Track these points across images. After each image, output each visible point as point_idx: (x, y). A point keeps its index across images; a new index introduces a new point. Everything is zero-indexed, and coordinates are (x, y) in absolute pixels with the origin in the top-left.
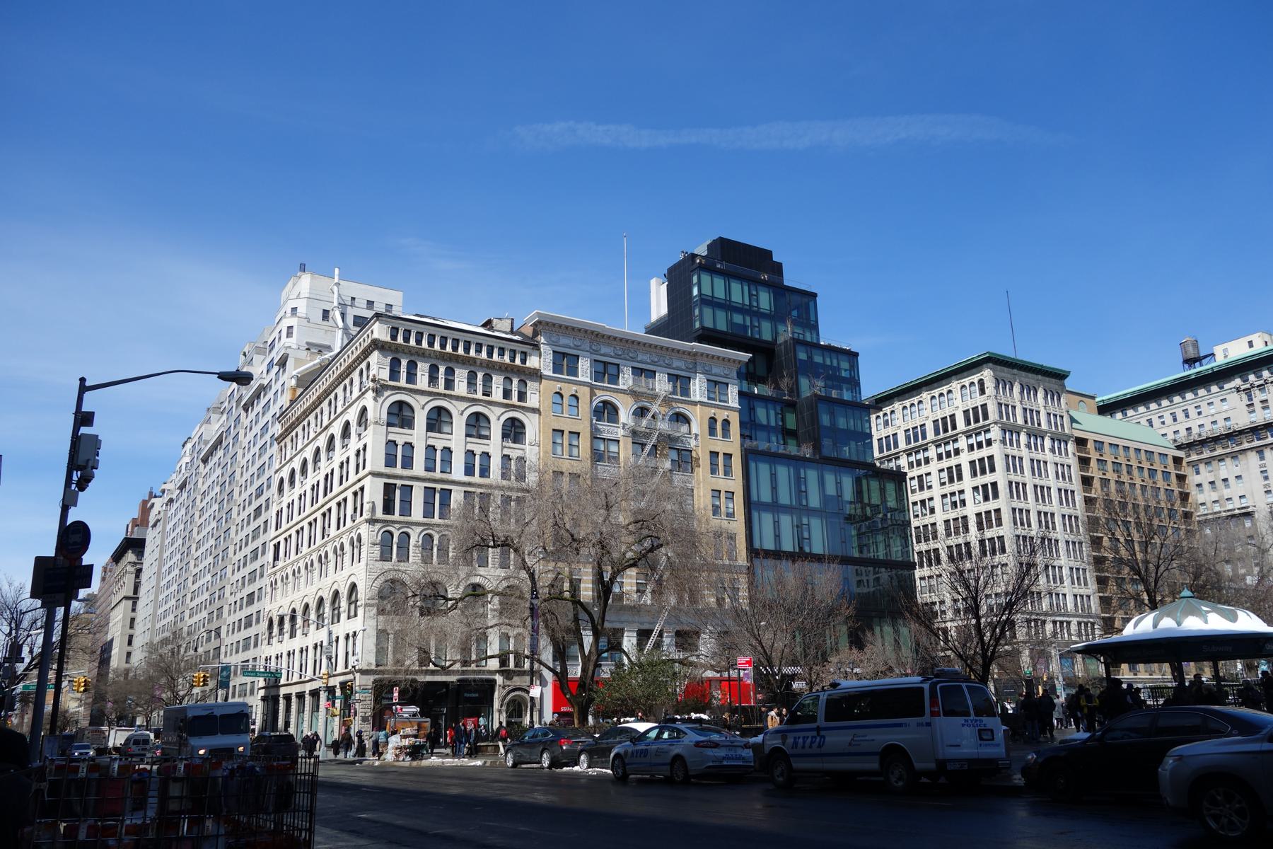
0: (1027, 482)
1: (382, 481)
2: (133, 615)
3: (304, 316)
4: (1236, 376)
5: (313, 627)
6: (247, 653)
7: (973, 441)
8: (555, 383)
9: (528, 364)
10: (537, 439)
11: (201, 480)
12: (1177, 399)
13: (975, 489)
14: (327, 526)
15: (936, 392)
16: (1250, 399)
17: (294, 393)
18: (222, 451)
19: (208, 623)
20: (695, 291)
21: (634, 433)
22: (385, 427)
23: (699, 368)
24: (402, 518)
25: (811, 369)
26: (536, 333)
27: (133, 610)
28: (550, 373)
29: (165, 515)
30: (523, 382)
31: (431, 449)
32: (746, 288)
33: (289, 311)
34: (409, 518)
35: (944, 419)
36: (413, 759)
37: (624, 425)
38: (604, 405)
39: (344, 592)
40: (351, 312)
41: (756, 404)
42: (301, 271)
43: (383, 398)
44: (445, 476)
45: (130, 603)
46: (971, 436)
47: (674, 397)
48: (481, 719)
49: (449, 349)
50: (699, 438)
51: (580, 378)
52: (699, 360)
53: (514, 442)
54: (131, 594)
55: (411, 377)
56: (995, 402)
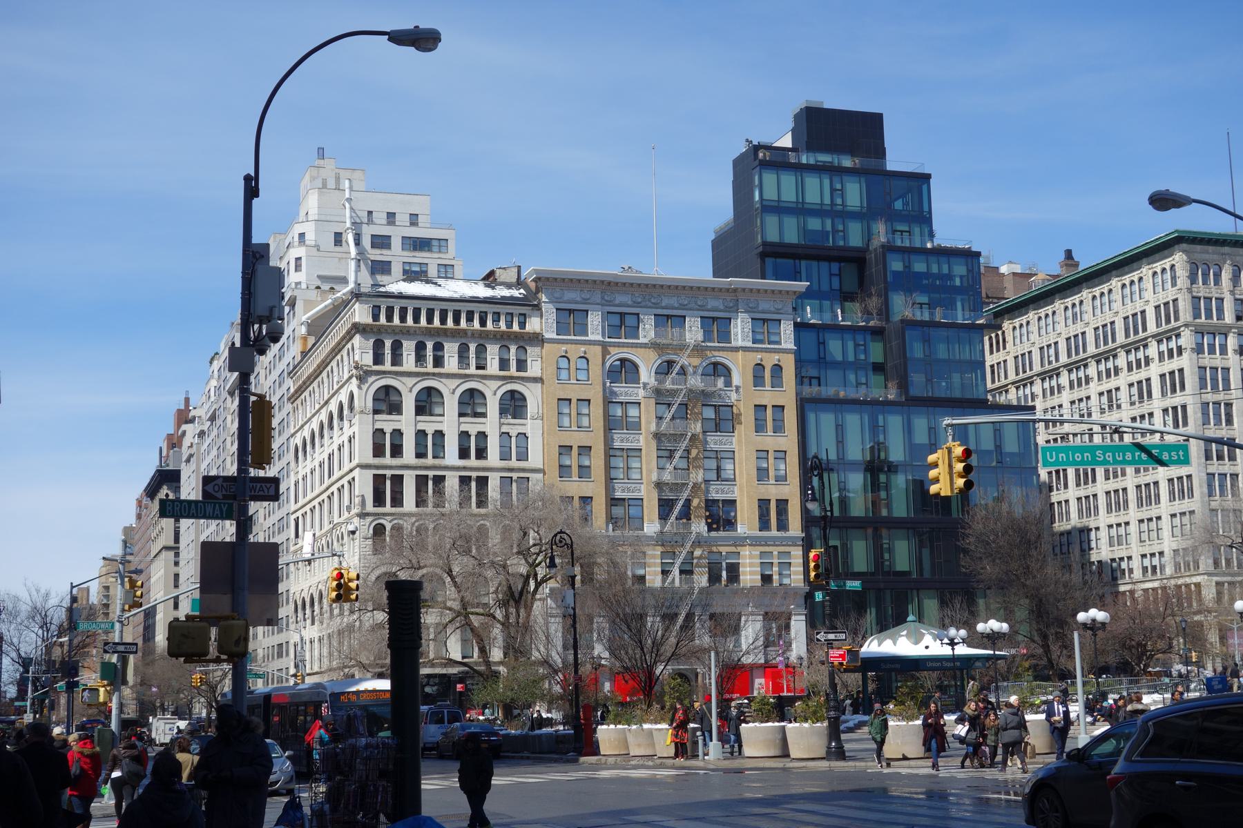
2: (176, 570)
6: (281, 635)
10: (540, 411)
13: (1165, 411)
17: (305, 343)
21: (658, 392)
22: (371, 415)
25: (909, 282)
27: (176, 564)
29: (198, 450)
30: (522, 348)
31: (421, 434)
32: (827, 182)
37: (645, 385)
38: (621, 363)
40: (367, 232)
41: (828, 335)
44: (437, 462)
45: (171, 554)
47: (709, 344)
50: (741, 390)
51: (591, 337)
53: (514, 418)
54: (171, 543)
56: (1188, 297)
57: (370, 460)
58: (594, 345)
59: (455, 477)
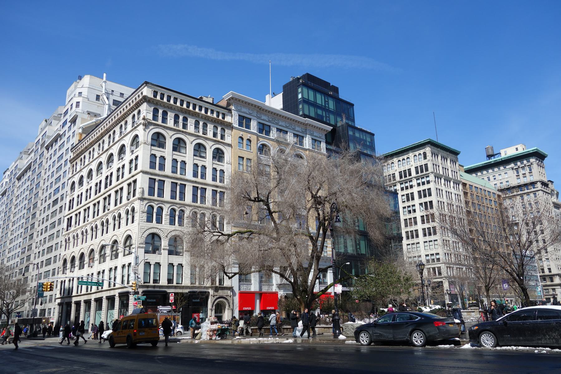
0: (445, 202)
1: (148, 177)
3: (86, 97)
4: (512, 163)
5: (77, 268)
7: (403, 186)
8: (240, 132)
9: (226, 120)
10: (231, 161)
11: (16, 189)
12: (485, 172)
13: (421, 204)
14: (87, 215)
15: (401, 158)
16: (518, 173)
18: (31, 172)
19: (20, 264)
20: (300, 96)
22: (150, 146)
23: (308, 132)
24: (159, 199)
26: (229, 104)
28: (237, 126)
31: (175, 161)
32: (323, 97)
33: (77, 94)
34: (163, 199)
35: (405, 171)
36: (222, 339)
39: (121, 240)
40: (112, 98)
42: (79, 79)
43: (149, 130)
44: (182, 177)
46: (403, 183)
48: (201, 314)
49: (185, 106)
51: (252, 130)
52: (308, 128)
53: (219, 161)
55: (164, 120)
57: (148, 169)
58: (254, 135)
59: (191, 186)
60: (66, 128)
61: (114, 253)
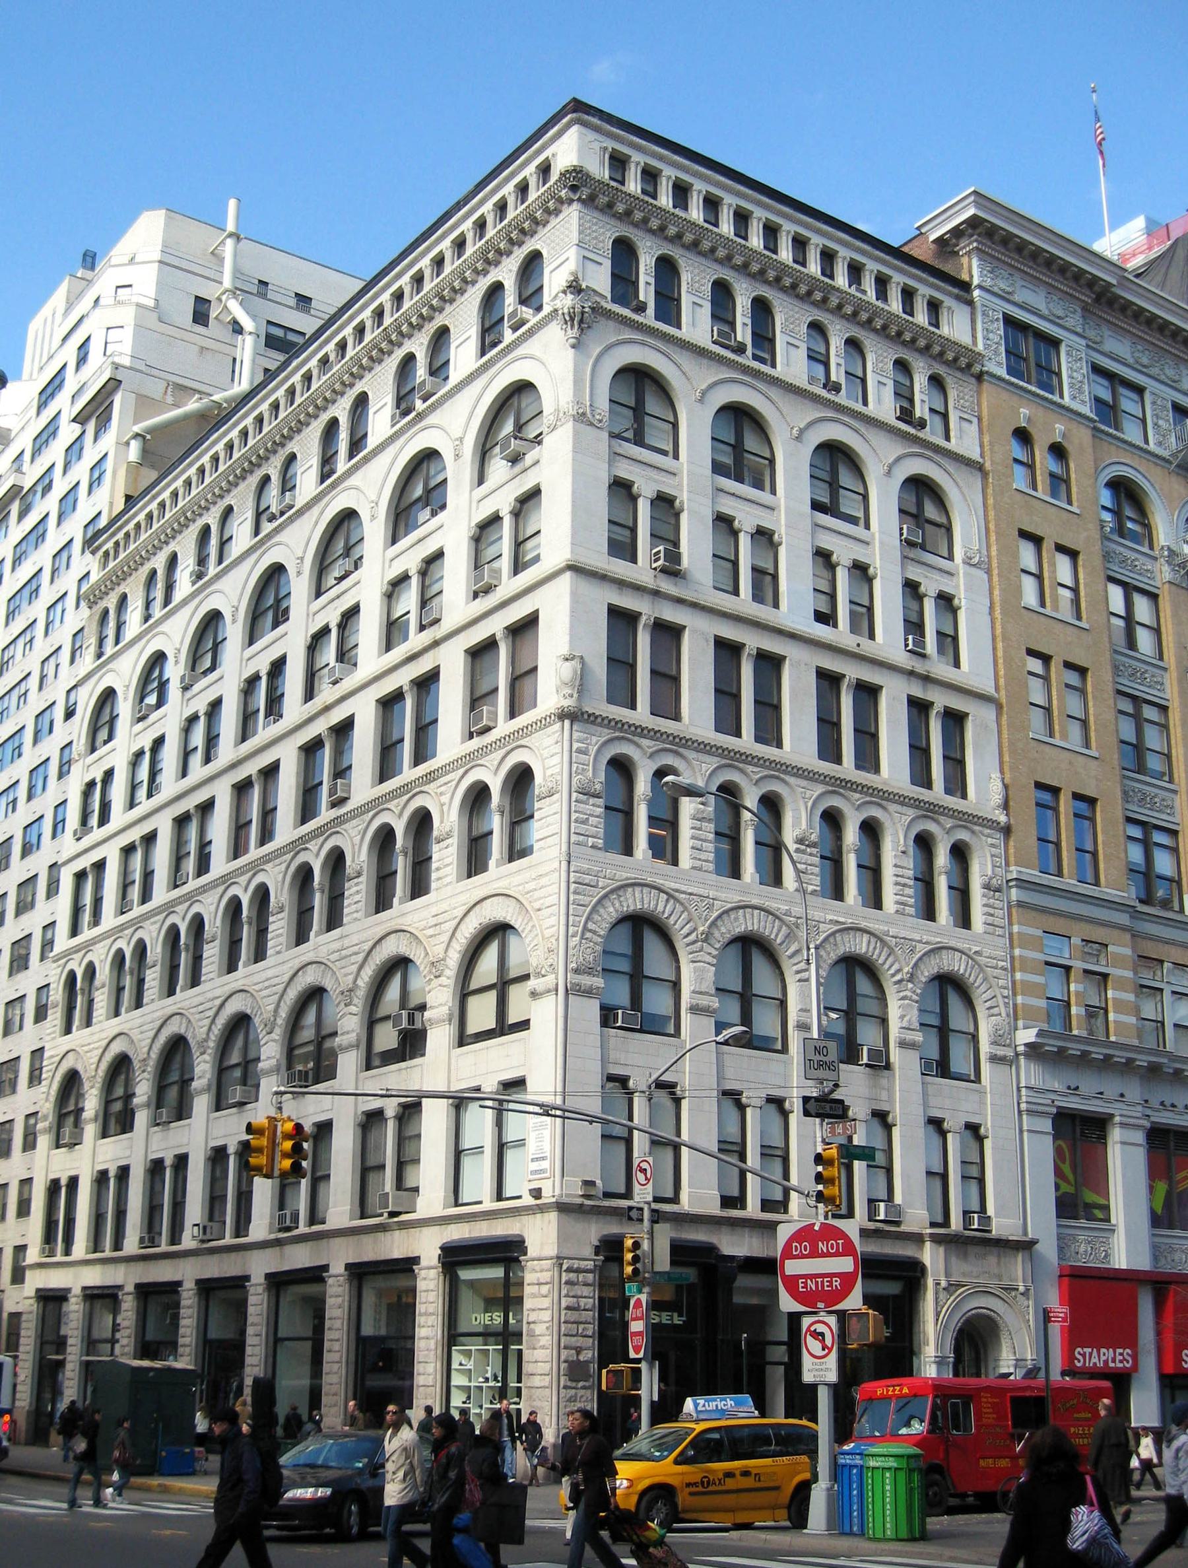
28: (1002, 372)
42: (84, 267)
44: (763, 612)
60: (55, 452)
61: (117, 1107)
